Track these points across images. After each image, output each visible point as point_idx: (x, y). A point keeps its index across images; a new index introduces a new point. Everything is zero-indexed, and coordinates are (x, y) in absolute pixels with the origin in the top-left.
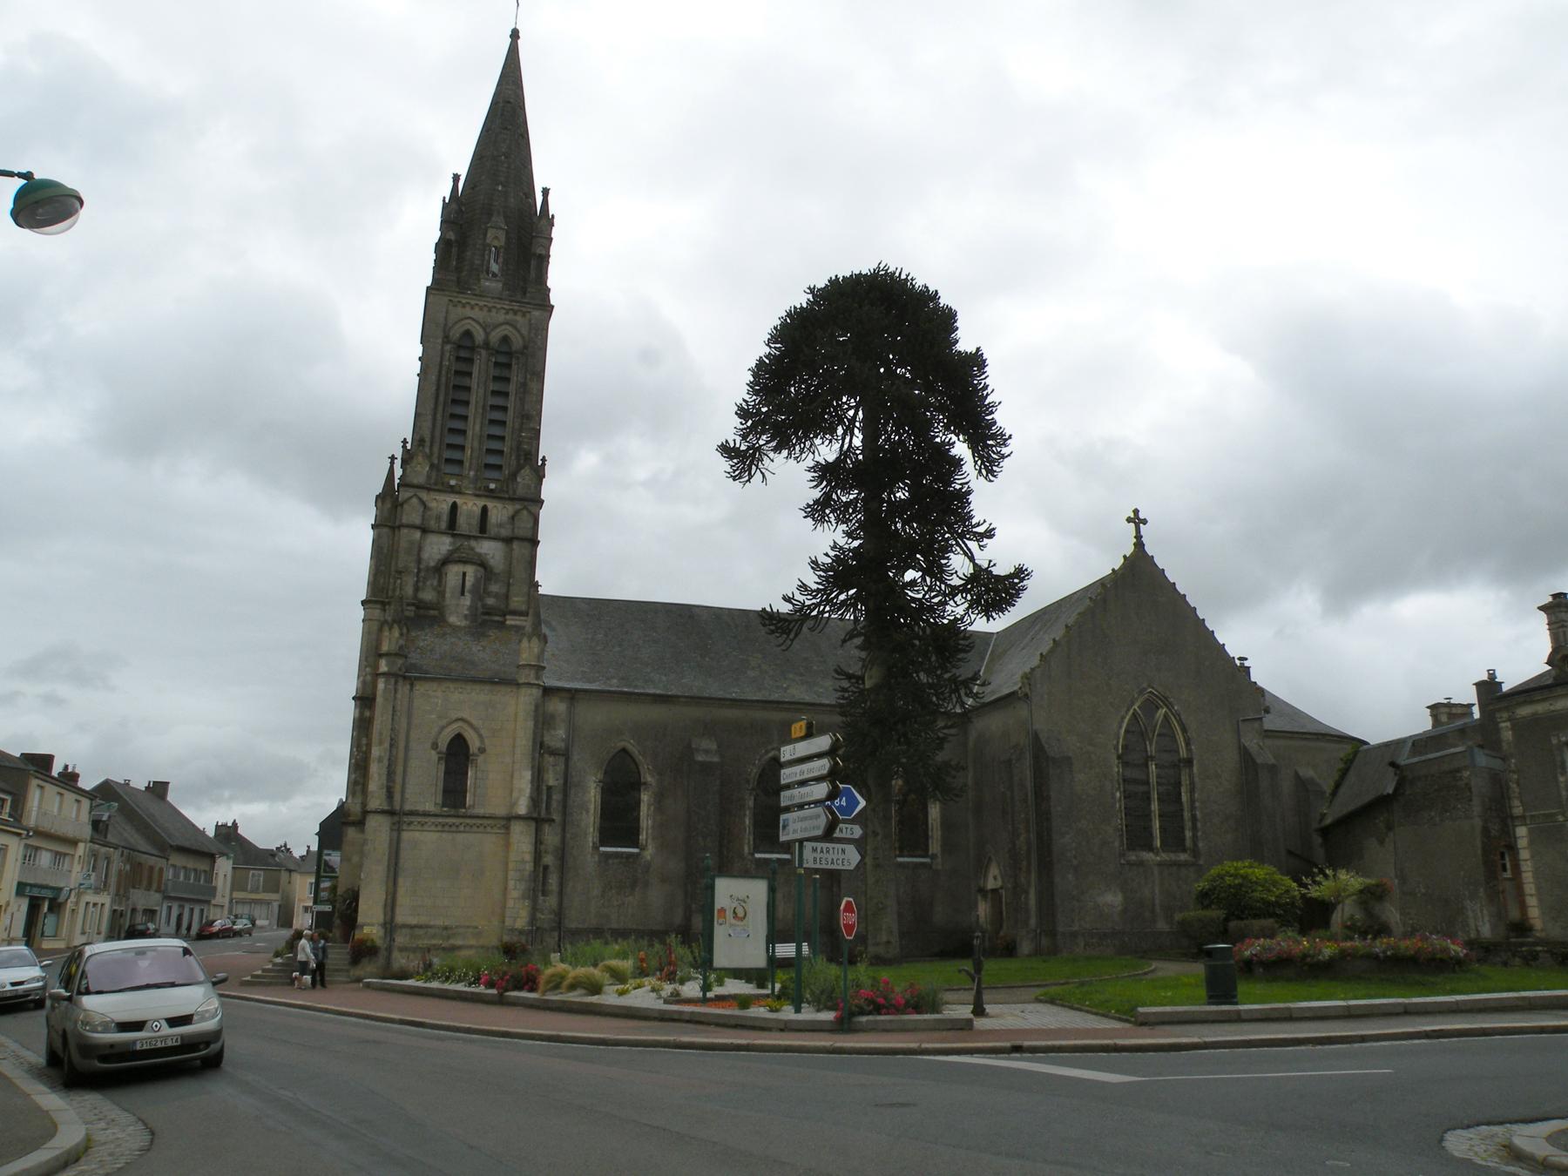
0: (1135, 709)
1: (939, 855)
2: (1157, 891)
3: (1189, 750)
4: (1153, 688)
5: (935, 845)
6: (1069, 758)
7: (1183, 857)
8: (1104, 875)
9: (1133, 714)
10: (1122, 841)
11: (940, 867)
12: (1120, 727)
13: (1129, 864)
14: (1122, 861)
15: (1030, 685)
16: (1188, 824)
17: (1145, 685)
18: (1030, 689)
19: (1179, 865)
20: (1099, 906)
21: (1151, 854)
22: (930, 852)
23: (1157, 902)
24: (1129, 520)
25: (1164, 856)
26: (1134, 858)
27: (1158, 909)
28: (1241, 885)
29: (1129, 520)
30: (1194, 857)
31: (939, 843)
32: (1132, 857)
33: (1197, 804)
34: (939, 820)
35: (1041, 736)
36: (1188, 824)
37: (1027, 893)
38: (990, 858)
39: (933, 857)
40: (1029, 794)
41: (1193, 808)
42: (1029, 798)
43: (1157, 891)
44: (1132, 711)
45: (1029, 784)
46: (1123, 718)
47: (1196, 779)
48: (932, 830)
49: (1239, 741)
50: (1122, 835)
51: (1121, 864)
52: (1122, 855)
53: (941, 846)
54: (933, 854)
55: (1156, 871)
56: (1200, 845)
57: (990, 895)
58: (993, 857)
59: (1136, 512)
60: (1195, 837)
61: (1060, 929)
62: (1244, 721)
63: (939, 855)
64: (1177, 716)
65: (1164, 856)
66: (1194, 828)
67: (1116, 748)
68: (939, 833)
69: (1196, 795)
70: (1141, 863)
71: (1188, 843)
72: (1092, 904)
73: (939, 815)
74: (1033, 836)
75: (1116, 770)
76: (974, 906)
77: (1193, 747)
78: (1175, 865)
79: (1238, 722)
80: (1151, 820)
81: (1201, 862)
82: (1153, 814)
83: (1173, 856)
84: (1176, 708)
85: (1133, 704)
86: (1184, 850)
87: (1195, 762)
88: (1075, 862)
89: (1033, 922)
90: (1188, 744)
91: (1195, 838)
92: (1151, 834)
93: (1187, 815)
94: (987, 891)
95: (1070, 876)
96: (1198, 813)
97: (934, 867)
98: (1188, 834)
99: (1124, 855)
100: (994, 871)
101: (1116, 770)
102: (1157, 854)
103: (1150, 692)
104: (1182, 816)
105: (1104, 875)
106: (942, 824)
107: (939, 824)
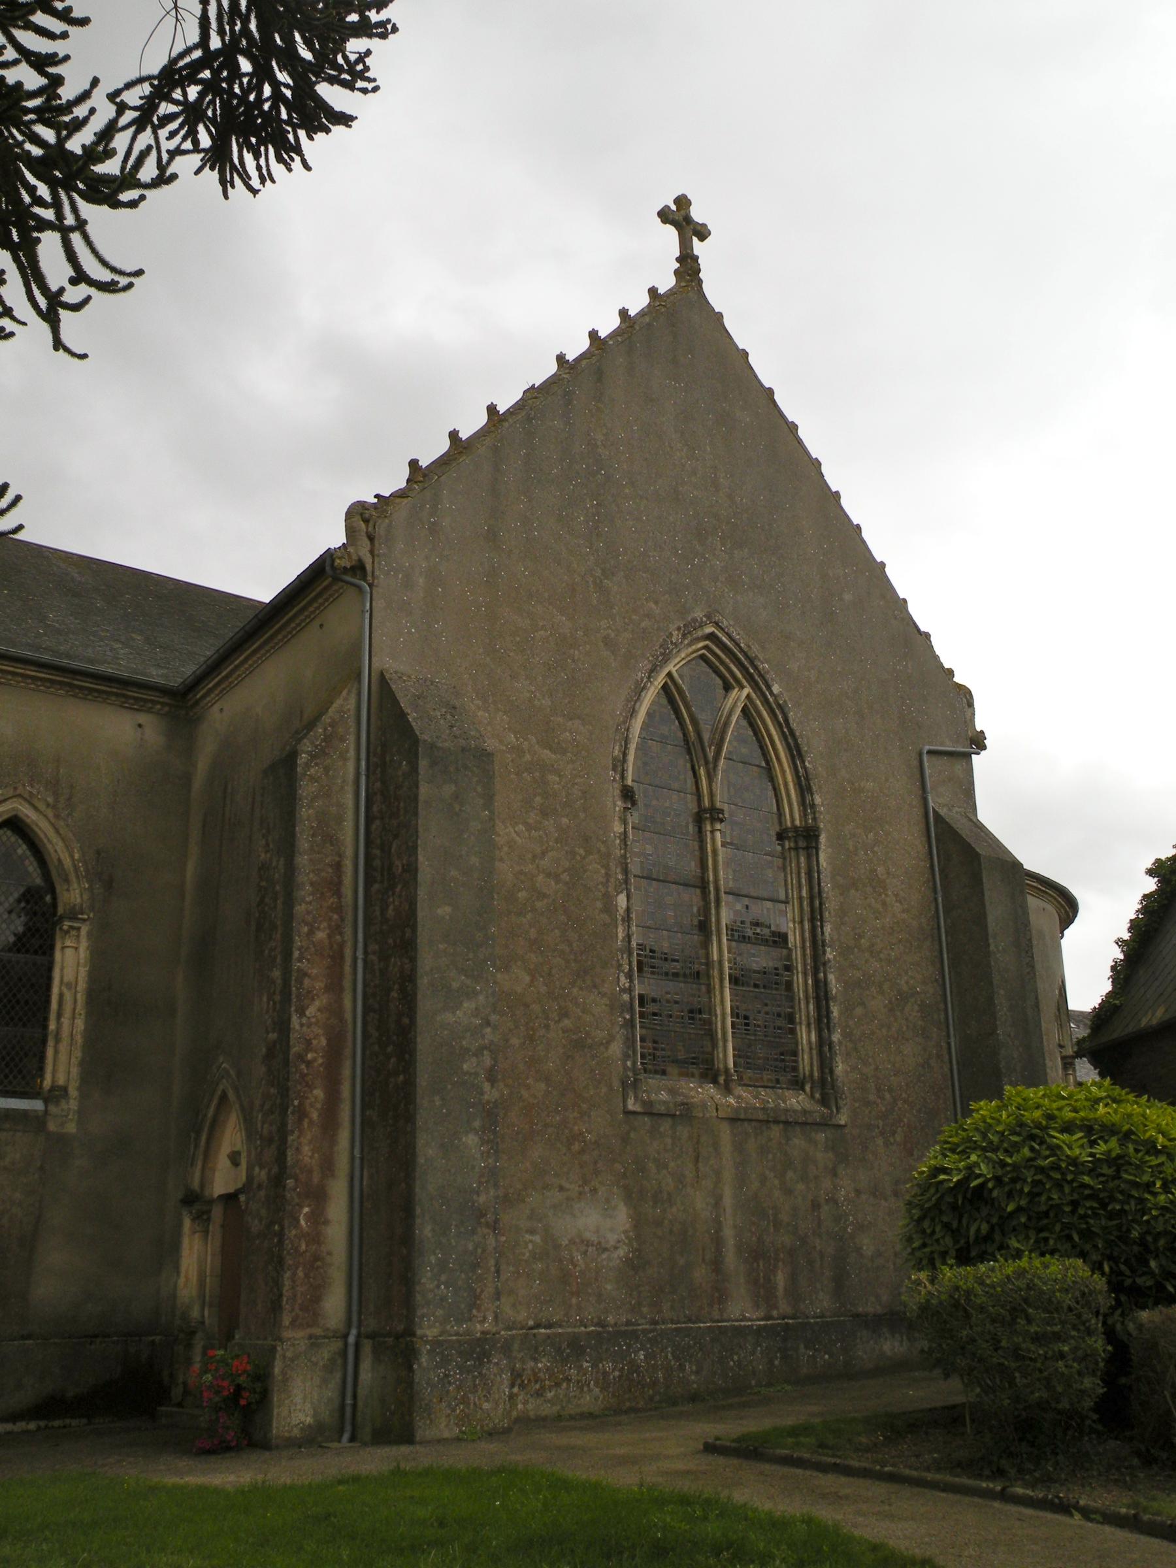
0: (669, 675)
1: (73, 1092)
2: (728, 1201)
3: (806, 805)
4: (717, 624)
5: (63, 1057)
6: (484, 757)
7: (796, 1101)
8: (576, 1147)
9: (665, 687)
10: (630, 1042)
11: (71, 1128)
12: (633, 712)
13: (649, 1111)
14: (631, 1105)
15: (371, 538)
16: (806, 1010)
17: (699, 614)
18: (372, 552)
19: (788, 1123)
20: (557, 1247)
21: (711, 1089)
22: (47, 1083)
23: (728, 1233)
24: (665, 216)
25: (743, 1097)
26: (664, 1096)
27: (730, 1258)
28: (1118, 1163)
29: (665, 216)
30: (824, 1101)
31: (78, 1054)
32: (659, 1091)
33: (830, 954)
34: (82, 986)
35: (387, 676)
36: (806, 1010)
37: (319, 1197)
38: (224, 1097)
39: (57, 1094)
40: (348, 864)
41: (818, 963)
42: (348, 879)
43: (728, 1201)
44: (660, 679)
45: (349, 834)
46: (640, 690)
47: (827, 886)
48: (59, 1015)
49: (925, 801)
50: (630, 1024)
51: (627, 1113)
52: (630, 1085)
53: (82, 1064)
54: (53, 1088)
55: (726, 1133)
56: (840, 1068)
57: (217, 1212)
58: (231, 1095)
59: (682, 202)
60: (824, 1046)
61: (428, 1329)
62: (930, 752)
63: (73, 1092)
64: (778, 711)
65: (743, 1097)
66: (823, 1021)
67: (619, 764)
68: (80, 1024)
69: (828, 929)
70: (684, 1113)
71: (806, 1062)
72: (537, 1238)
73: (83, 972)
74: (351, 1005)
75: (618, 828)
76: (169, 1251)
77: (818, 800)
78: (776, 1122)
79: (920, 755)
80: (710, 990)
81: (843, 1119)
82: (715, 973)
83: (768, 1098)
84: (776, 689)
85: (666, 659)
86: (797, 1084)
87: (823, 839)
88: (490, 1094)
89: (334, 1305)
90: (804, 788)
91: (824, 1046)
92: (711, 1034)
93: (801, 982)
94: (211, 1202)
95: (471, 1140)
96: (831, 977)
97: (52, 1126)
98: (806, 1036)
99: (636, 1084)
100: (232, 1137)
101: (618, 828)
102: (727, 1089)
103: (711, 637)
104: (789, 985)
105: (576, 1147)
106: (92, 996)
107: (81, 998)
